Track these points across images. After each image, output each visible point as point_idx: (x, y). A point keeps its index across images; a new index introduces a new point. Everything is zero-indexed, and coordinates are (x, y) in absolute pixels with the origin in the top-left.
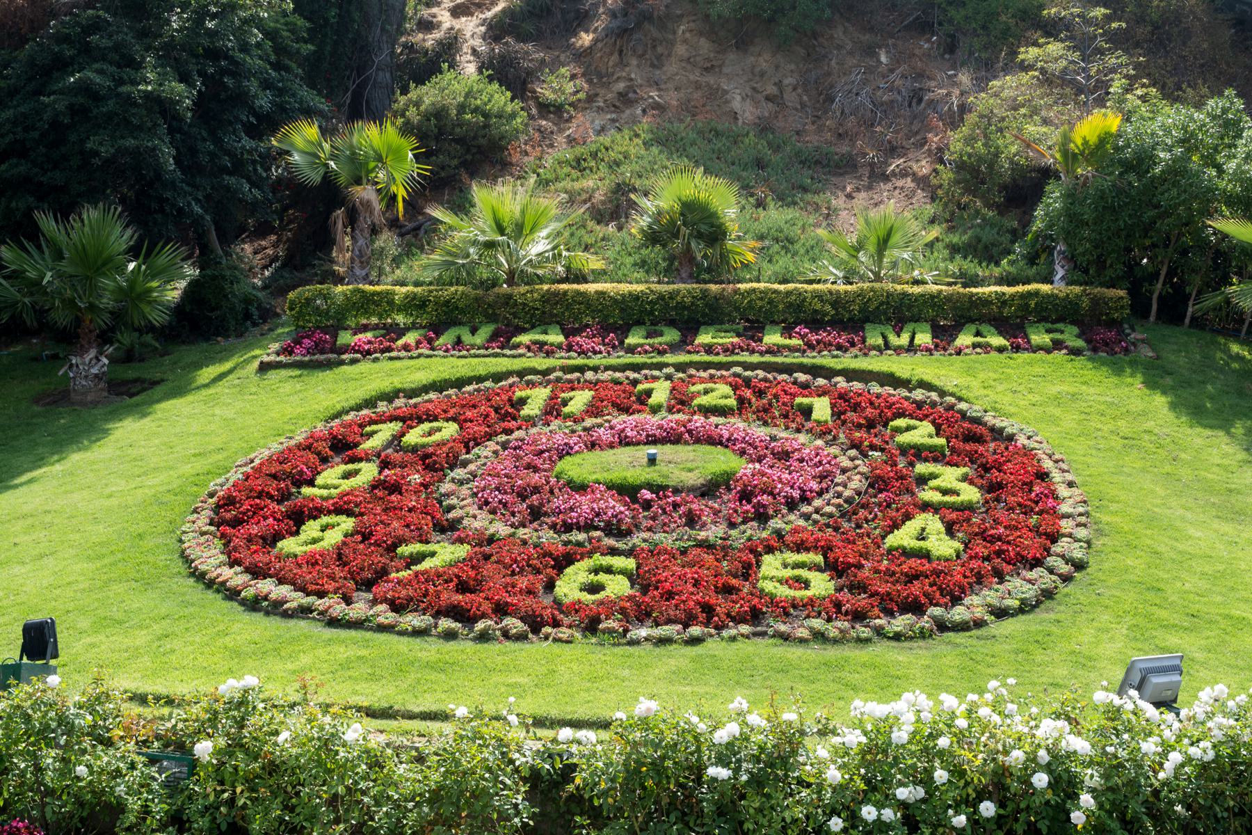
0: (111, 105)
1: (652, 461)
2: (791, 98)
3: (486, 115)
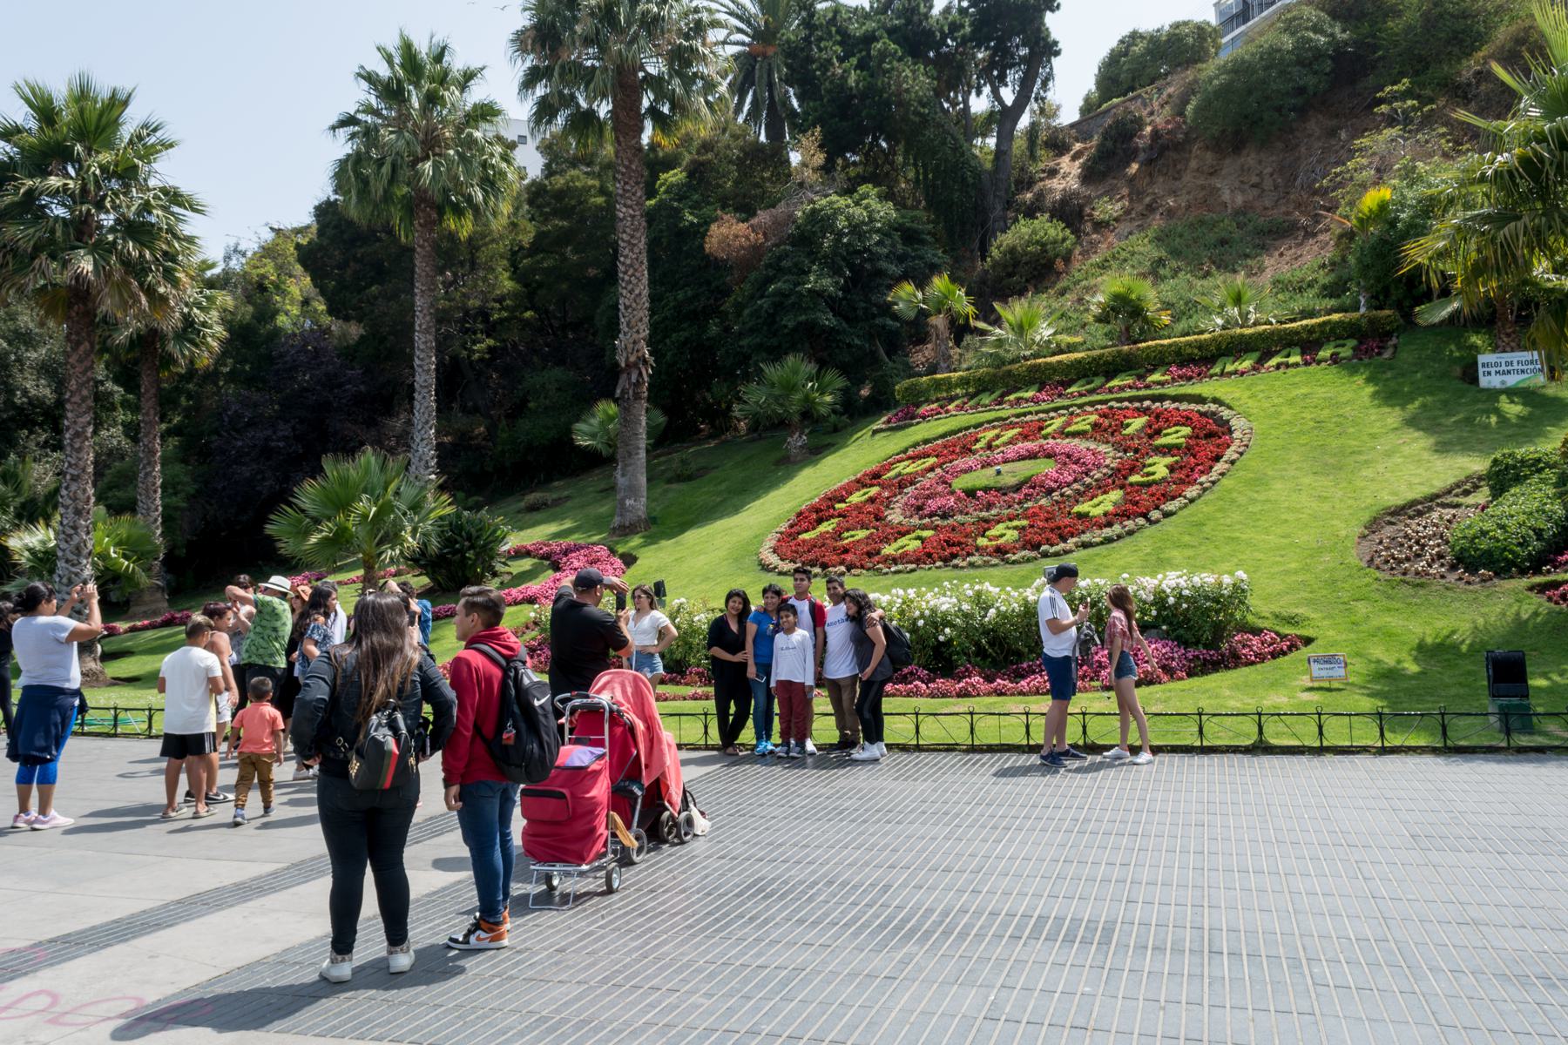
0: (793, 299)
1: (999, 473)
2: (1268, 184)
3: (1043, 245)
